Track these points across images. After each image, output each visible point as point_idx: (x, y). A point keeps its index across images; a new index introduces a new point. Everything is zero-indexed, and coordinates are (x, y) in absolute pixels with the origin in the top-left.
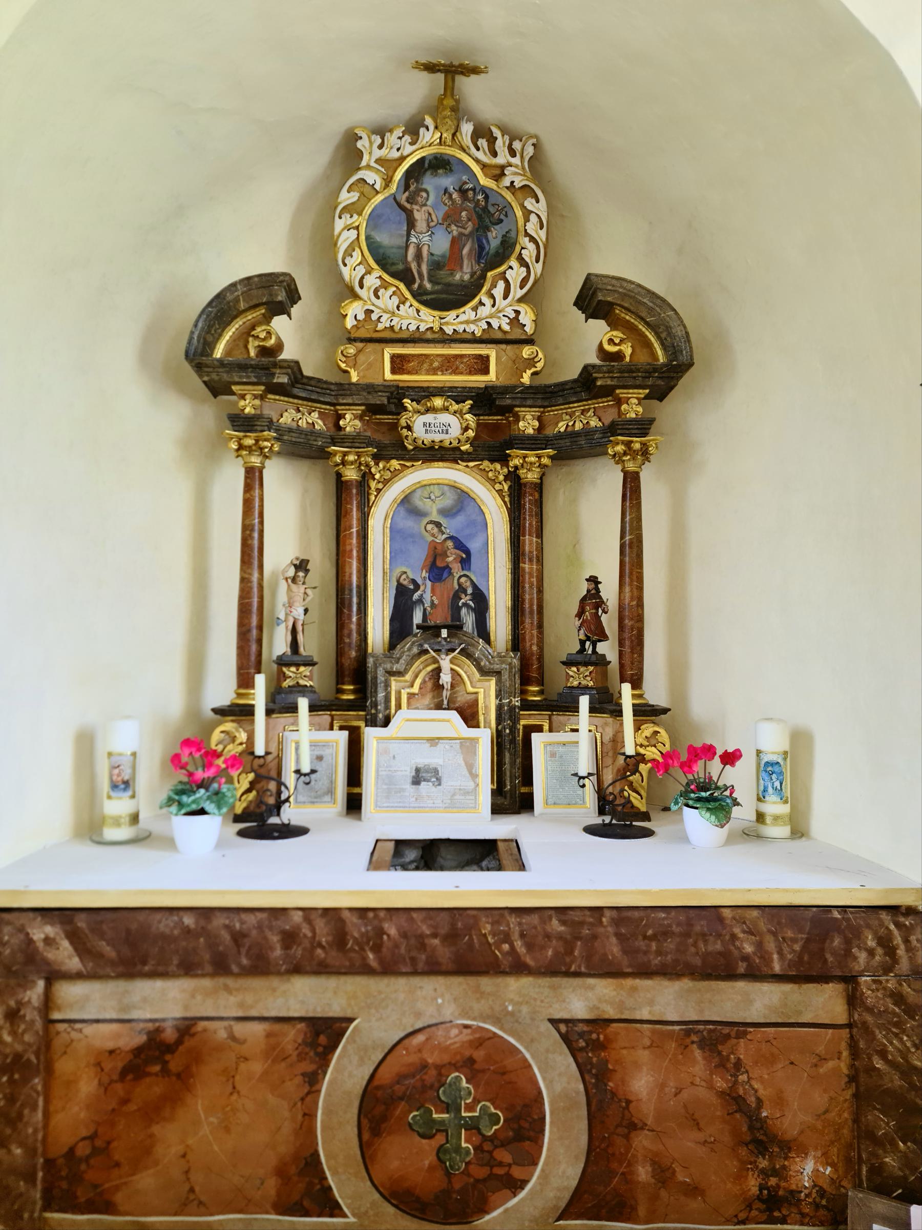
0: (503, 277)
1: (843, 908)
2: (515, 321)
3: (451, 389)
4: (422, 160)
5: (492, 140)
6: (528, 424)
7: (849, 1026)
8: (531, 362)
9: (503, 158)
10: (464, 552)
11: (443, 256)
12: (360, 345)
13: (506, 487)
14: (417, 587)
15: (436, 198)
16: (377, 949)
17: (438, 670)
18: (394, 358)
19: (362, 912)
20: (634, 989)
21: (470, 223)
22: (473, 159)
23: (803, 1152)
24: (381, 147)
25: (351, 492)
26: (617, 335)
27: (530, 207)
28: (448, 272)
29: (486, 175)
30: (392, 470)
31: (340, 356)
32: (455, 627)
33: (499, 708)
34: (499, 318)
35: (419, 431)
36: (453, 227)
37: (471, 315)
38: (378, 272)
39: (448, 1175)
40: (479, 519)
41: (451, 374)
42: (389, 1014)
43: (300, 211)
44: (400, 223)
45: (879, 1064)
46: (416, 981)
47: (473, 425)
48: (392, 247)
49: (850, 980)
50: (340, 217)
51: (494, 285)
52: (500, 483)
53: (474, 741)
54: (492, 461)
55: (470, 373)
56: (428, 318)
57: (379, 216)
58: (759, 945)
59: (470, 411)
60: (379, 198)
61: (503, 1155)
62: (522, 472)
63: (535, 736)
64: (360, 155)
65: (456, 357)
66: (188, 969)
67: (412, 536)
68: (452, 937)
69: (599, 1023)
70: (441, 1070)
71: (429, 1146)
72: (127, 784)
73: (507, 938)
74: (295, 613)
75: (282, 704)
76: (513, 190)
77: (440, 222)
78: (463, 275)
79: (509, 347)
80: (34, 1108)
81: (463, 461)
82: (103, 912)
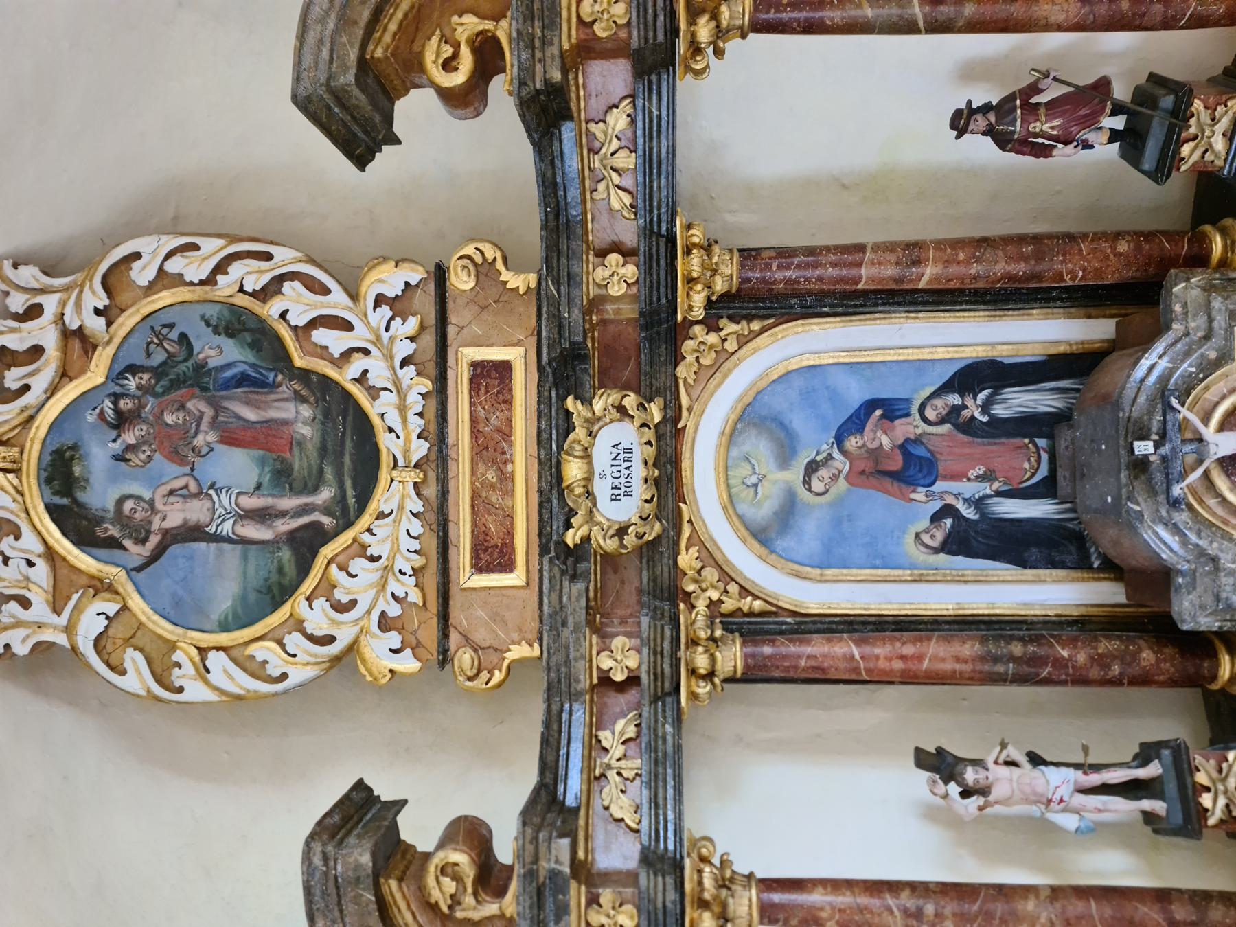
3: (542, 440)
4: (51, 510)
8: (484, 270)
9: (44, 333)
10: (869, 414)
11: (262, 463)
12: (454, 638)
13: (733, 327)
14: (947, 511)
15: (136, 479)
18: (480, 567)
21: (189, 405)
24: (25, 603)
25: (770, 657)
27: (151, 273)
28: (296, 450)
29: (83, 371)
30: (699, 565)
31: (479, 684)
34: (392, 339)
35: (627, 510)
36: (199, 441)
37: (387, 401)
38: (298, 604)
40: (798, 382)
41: (511, 444)
44: (191, 558)
47: (614, 397)
48: (245, 573)
50: (180, 690)
51: (323, 352)
52: (724, 340)
54: (676, 358)
55: (509, 402)
56: (396, 493)
57: (177, 603)
59: (588, 402)
60: (137, 604)
62: (720, 286)
65: (475, 432)
67: (837, 522)
74: (1065, 791)
76: (114, 311)
77: (187, 469)
78: (301, 419)
79: (453, 319)
81: (679, 418)
82: (90, 394)
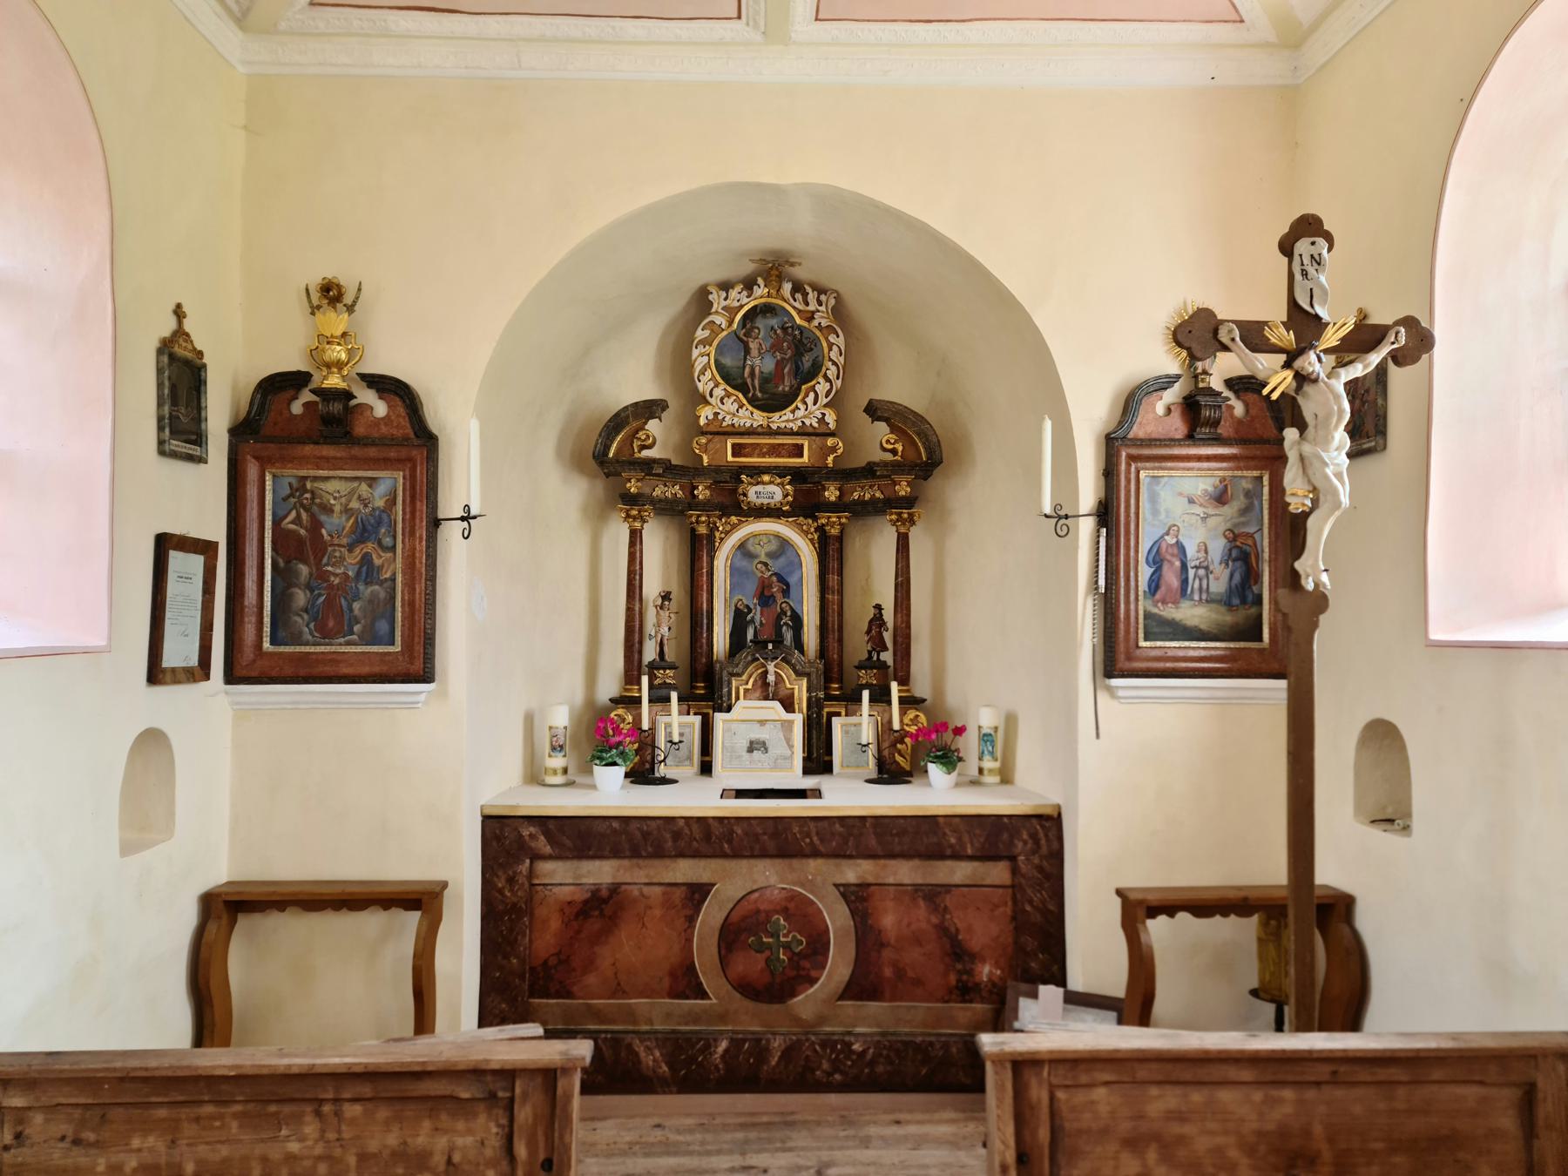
0: (813, 389)
1: (1010, 817)
2: (822, 420)
5: (805, 295)
6: (831, 494)
7: (1013, 886)
8: (834, 449)
16: (730, 842)
17: (766, 672)
18: (733, 446)
19: (720, 819)
20: (885, 866)
22: (793, 308)
23: (983, 961)
26: (893, 437)
32: (778, 642)
33: (809, 699)
38: (723, 385)
39: (772, 973)
42: (736, 881)
43: (665, 334)
45: (1028, 908)
46: (753, 861)
49: (1012, 859)
53: (791, 722)
54: (806, 517)
58: (959, 839)
61: (807, 964)
63: (834, 719)
64: (711, 304)
66: (616, 854)
67: (746, 573)
68: (775, 835)
69: (864, 886)
70: (769, 914)
71: (761, 957)
72: (561, 747)
73: (808, 835)
75: (660, 699)
78: (785, 386)
80: (524, 935)
